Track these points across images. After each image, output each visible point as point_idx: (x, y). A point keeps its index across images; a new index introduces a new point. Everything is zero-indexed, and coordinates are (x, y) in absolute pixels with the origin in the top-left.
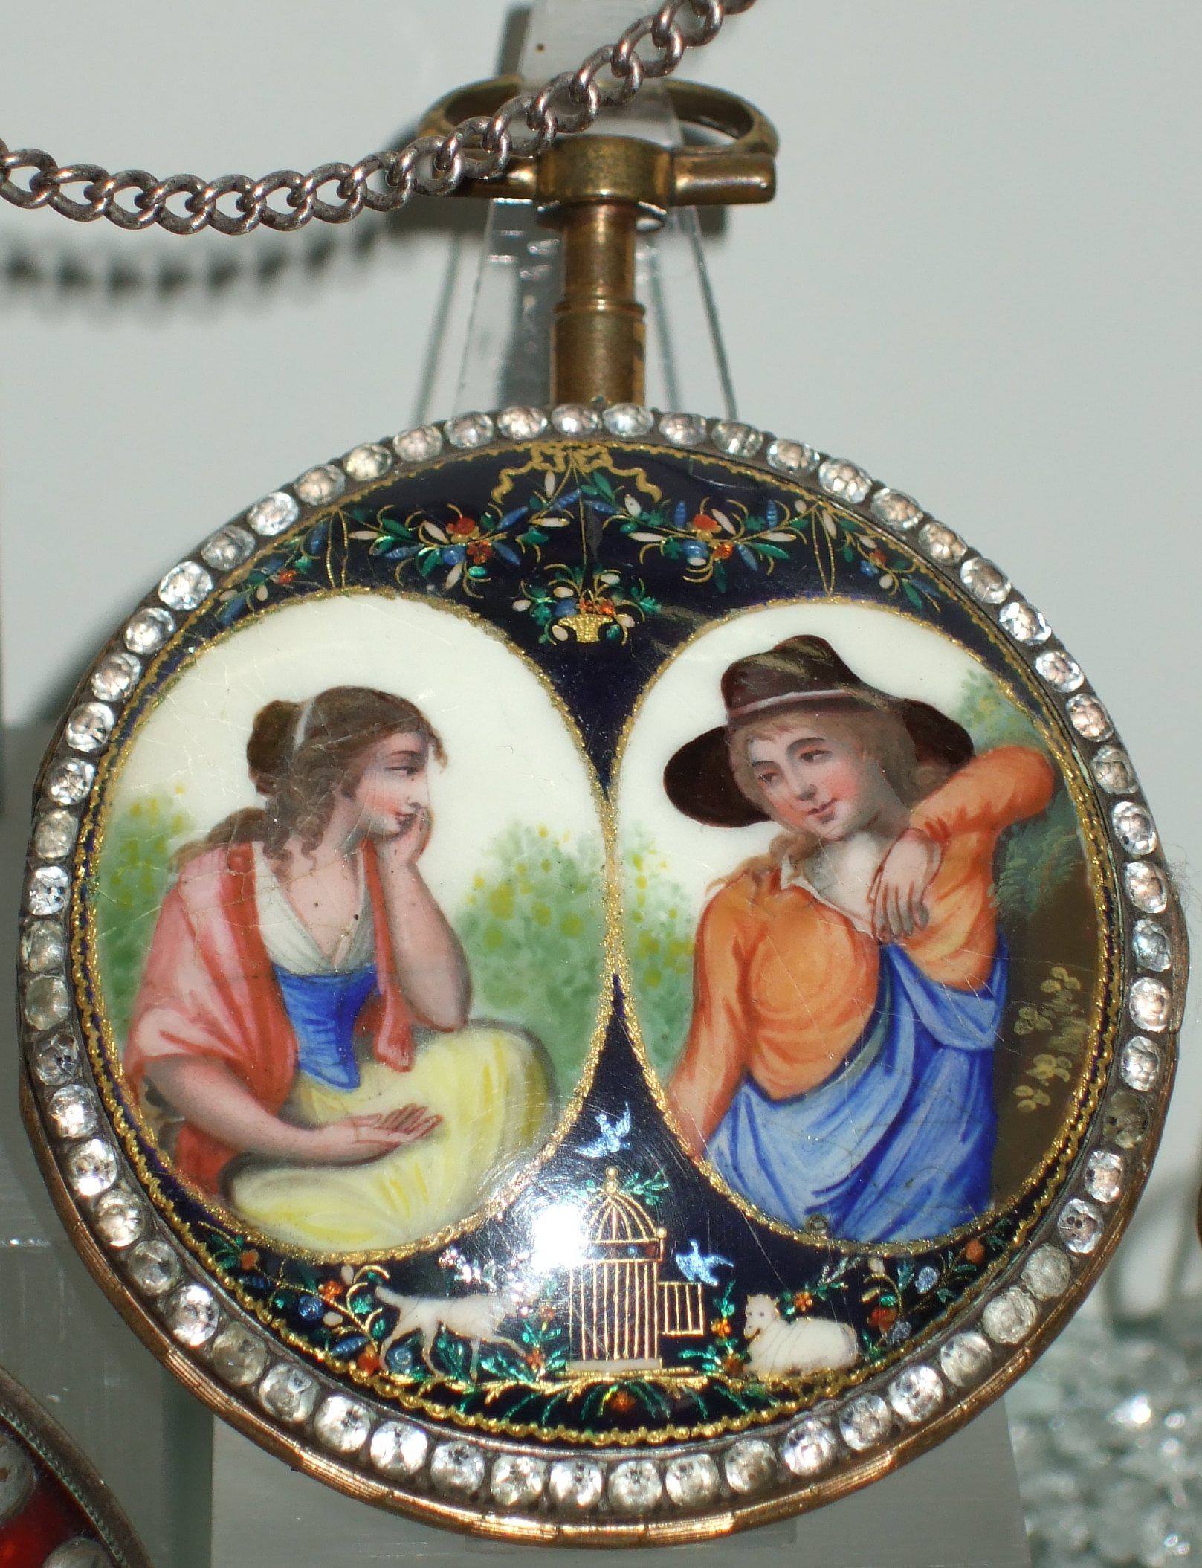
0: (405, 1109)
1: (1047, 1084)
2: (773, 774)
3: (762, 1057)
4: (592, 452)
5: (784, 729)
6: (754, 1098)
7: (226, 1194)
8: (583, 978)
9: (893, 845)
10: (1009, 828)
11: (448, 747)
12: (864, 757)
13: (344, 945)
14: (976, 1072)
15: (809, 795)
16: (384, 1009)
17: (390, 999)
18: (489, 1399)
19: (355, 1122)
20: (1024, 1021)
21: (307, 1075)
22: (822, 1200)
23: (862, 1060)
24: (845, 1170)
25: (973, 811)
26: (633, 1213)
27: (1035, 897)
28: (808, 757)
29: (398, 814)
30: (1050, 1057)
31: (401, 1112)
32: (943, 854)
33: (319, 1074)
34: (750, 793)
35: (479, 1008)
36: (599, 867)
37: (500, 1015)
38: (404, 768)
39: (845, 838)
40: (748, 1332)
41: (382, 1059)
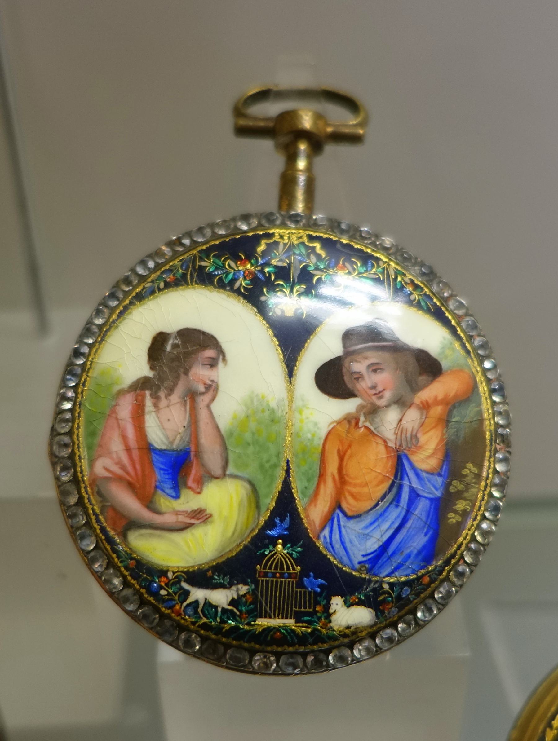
0: (198, 509)
1: (461, 512)
2: (360, 378)
3: (345, 498)
4: (300, 235)
5: (366, 358)
6: (341, 515)
7: (124, 535)
8: (274, 460)
9: (406, 411)
10: (455, 403)
11: (228, 356)
12: (398, 372)
13: (178, 437)
14: (433, 507)
15: (374, 387)
16: (192, 466)
17: (195, 462)
18: (224, 630)
19: (177, 513)
20: (454, 486)
21: (159, 492)
22: (365, 559)
23: (387, 501)
24: (376, 547)
25: (440, 397)
26: (289, 562)
27: (462, 434)
28: (375, 371)
29: (205, 384)
30: (463, 501)
31: (195, 511)
32: (426, 415)
33: (164, 491)
34: (349, 385)
35: (231, 470)
36: (284, 413)
37: (239, 474)
38: (209, 365)
39: (388, 406)
40: (331, 611)
41: (190, 488)
